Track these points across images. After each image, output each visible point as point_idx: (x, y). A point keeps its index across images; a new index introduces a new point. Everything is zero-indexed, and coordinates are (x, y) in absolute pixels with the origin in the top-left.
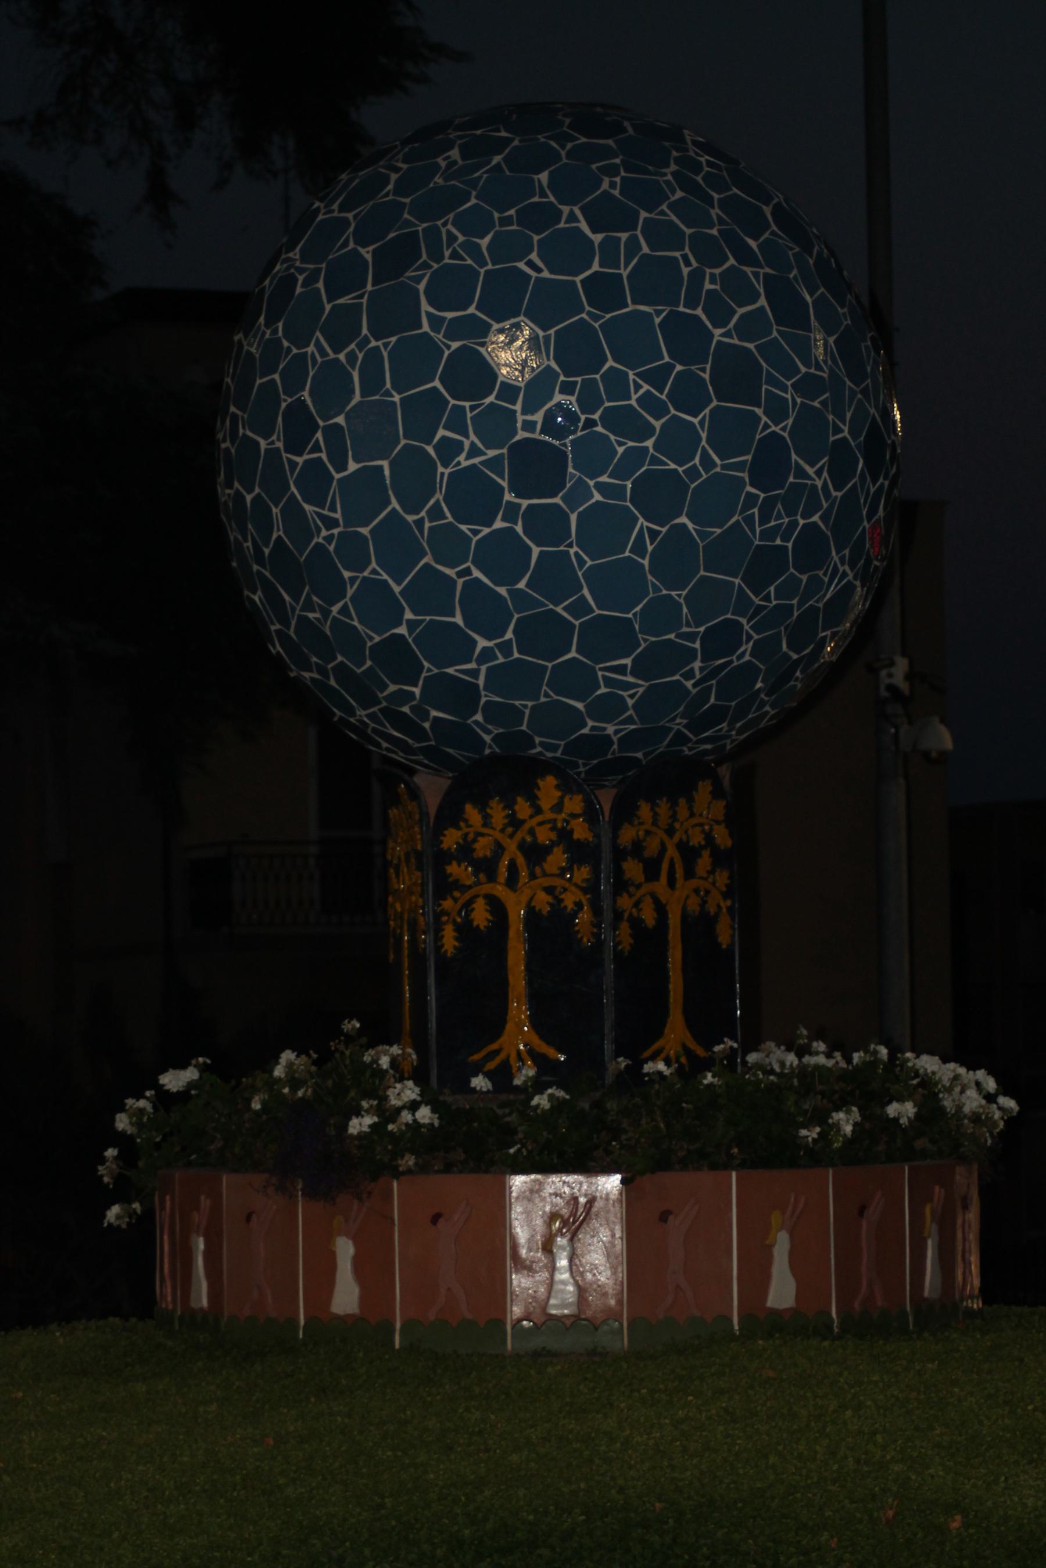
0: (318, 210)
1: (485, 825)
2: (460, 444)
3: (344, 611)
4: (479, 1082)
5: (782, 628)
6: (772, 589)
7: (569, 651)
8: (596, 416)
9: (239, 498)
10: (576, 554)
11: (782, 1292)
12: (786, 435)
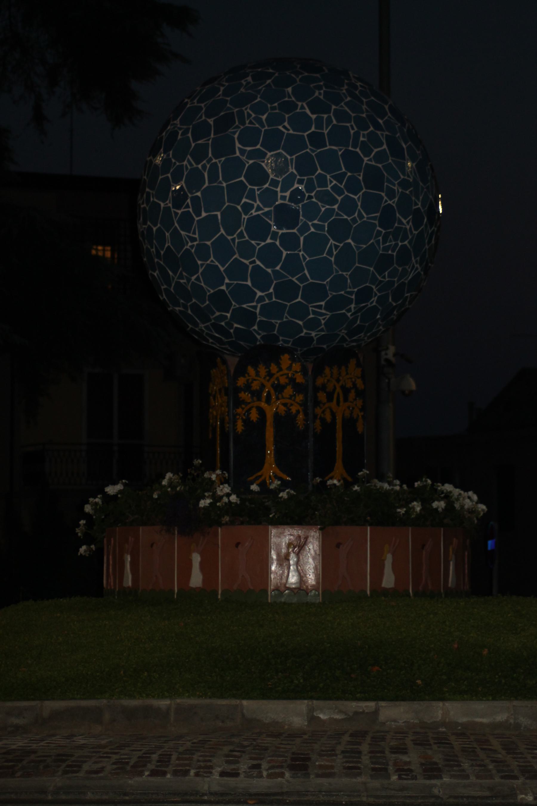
0: (187, 103)
1: (257, 376)
3: (198, 279)
4: (254, 487)
5: (390, 291)
7: (297, 298)
8: (313, 194)
9: (150, 229)
10: (303, 255)
12: (394, 205)
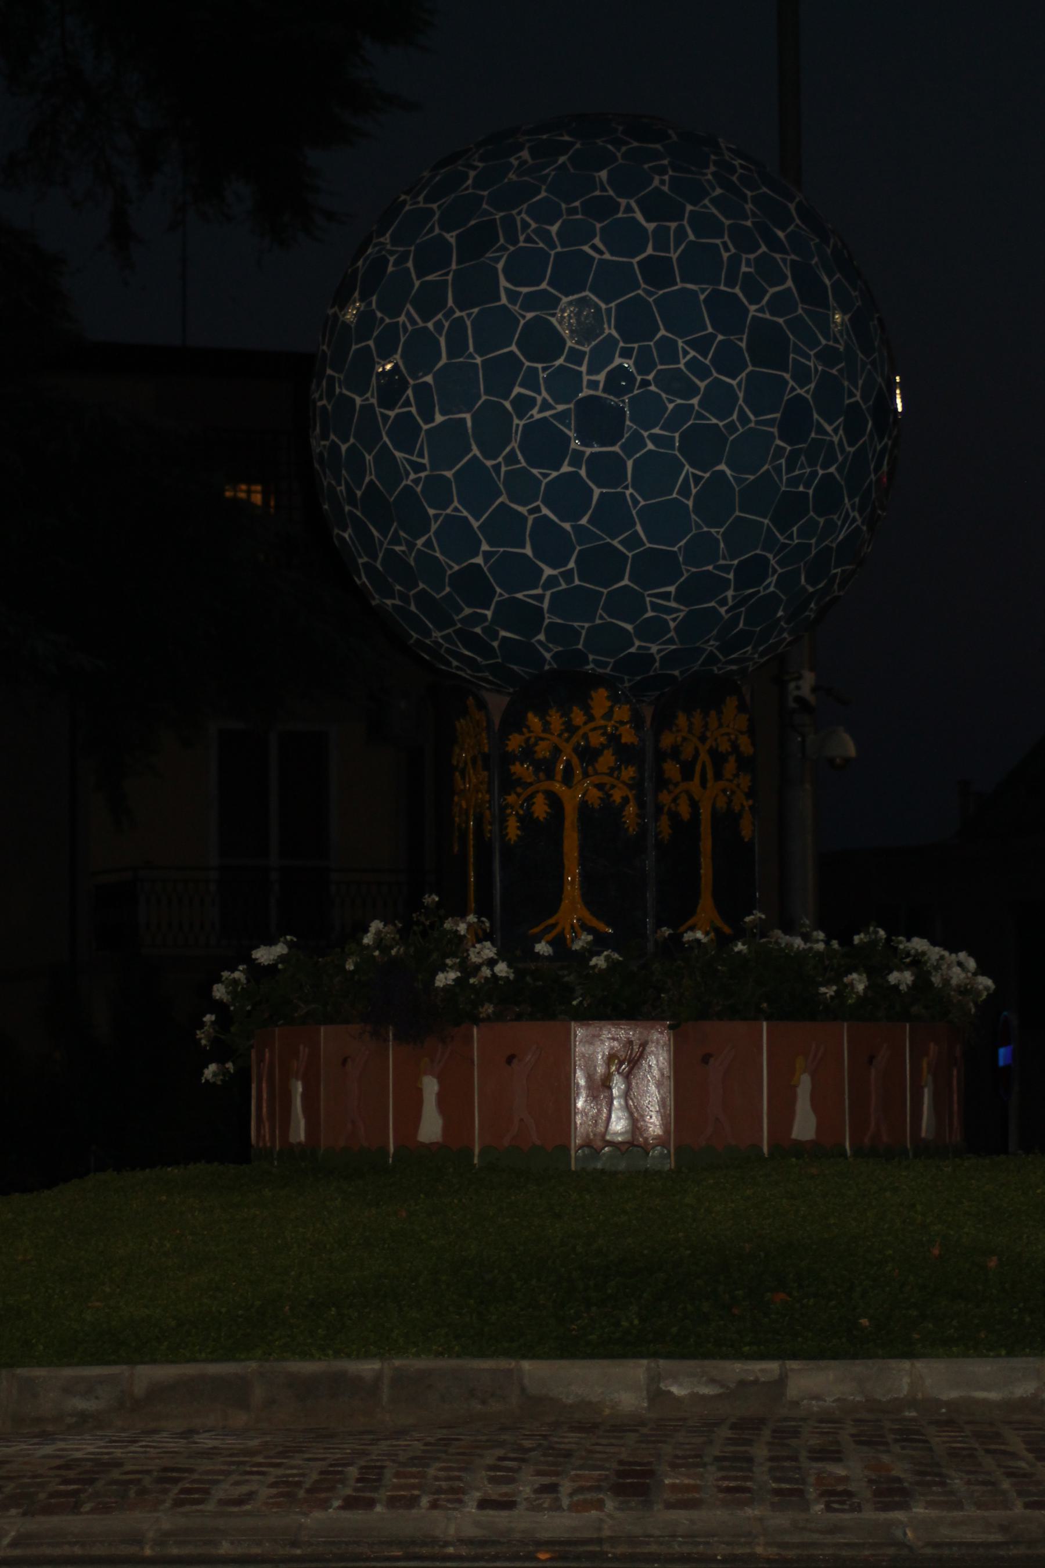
1: (544, 730)
2: (534, 400)
3: (428, 544)
4: (542, 948)
5: (802, 564)
6: (795, 529)
7: (622, 579)
8: (650, 377)
9: (334, 448)
11: (804, 1126)
12: (809, 397)
